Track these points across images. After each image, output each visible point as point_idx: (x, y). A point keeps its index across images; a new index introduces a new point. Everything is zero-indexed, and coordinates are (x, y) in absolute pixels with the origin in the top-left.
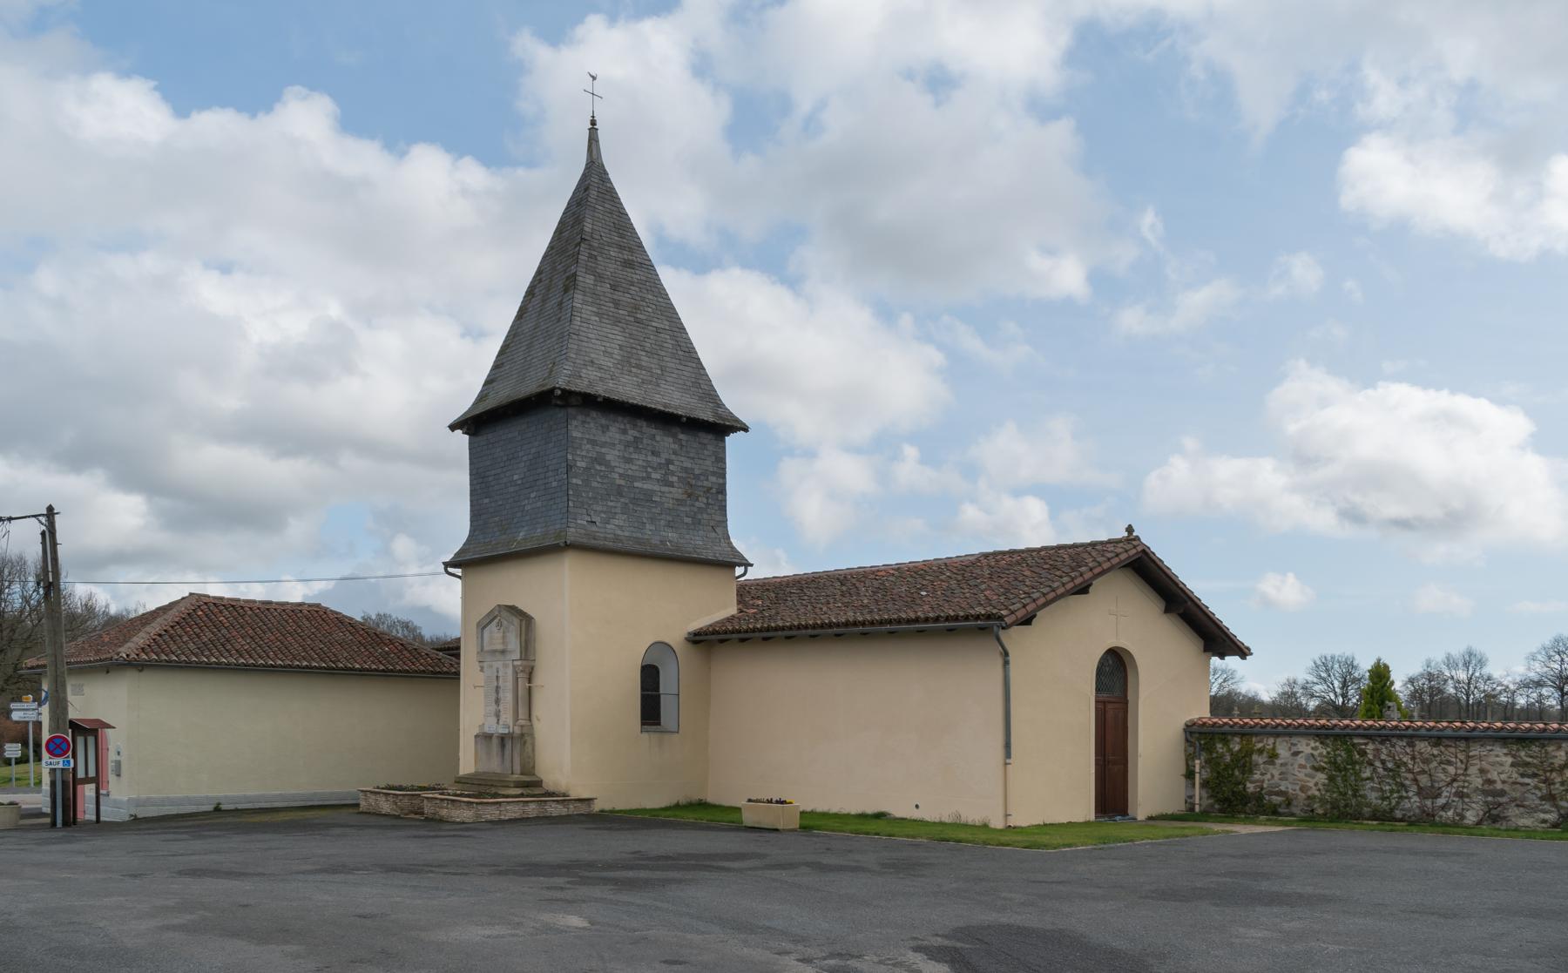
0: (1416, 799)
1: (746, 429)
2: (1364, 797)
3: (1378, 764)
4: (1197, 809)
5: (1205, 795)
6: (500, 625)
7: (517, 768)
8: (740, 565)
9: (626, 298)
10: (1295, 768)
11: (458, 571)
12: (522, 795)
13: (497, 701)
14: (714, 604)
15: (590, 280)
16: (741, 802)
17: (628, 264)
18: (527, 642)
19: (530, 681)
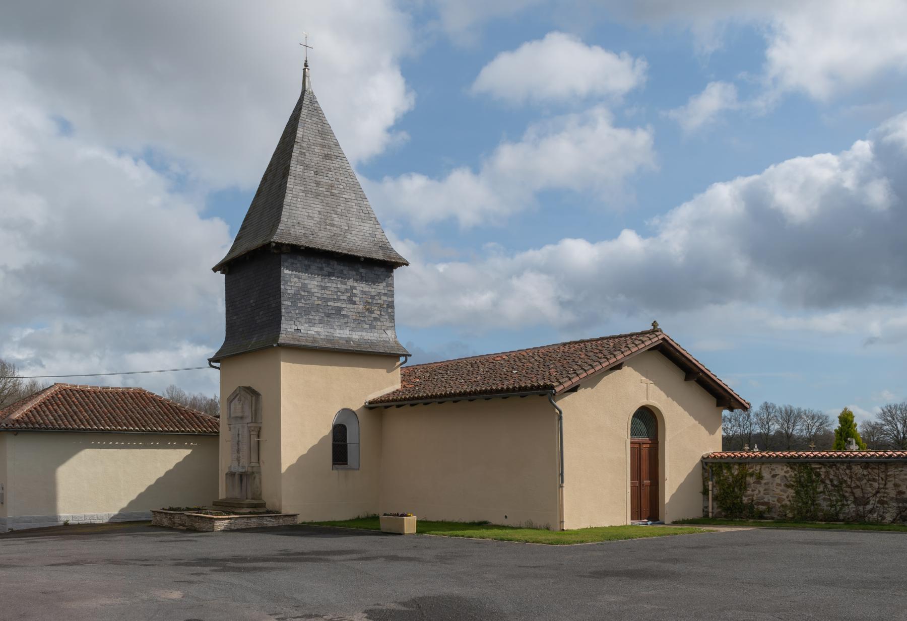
0: (853, 505)
1: (407, 265)
2: (819, 505)
3: (828, 482)
4: (710, 515)
5: (715, 506)
6: (240, 400)
7: (250, 496)
8: (403, 355)
9: (325, 180)
10: (773, 486)
11: (218, 365)
12: (250, 513)
13: (238, 451)
14: (386, 383)
15: (300, 168)
16: (380, 513)
17: (327, 157)
18: (256, 410)
19: (259, 437)
